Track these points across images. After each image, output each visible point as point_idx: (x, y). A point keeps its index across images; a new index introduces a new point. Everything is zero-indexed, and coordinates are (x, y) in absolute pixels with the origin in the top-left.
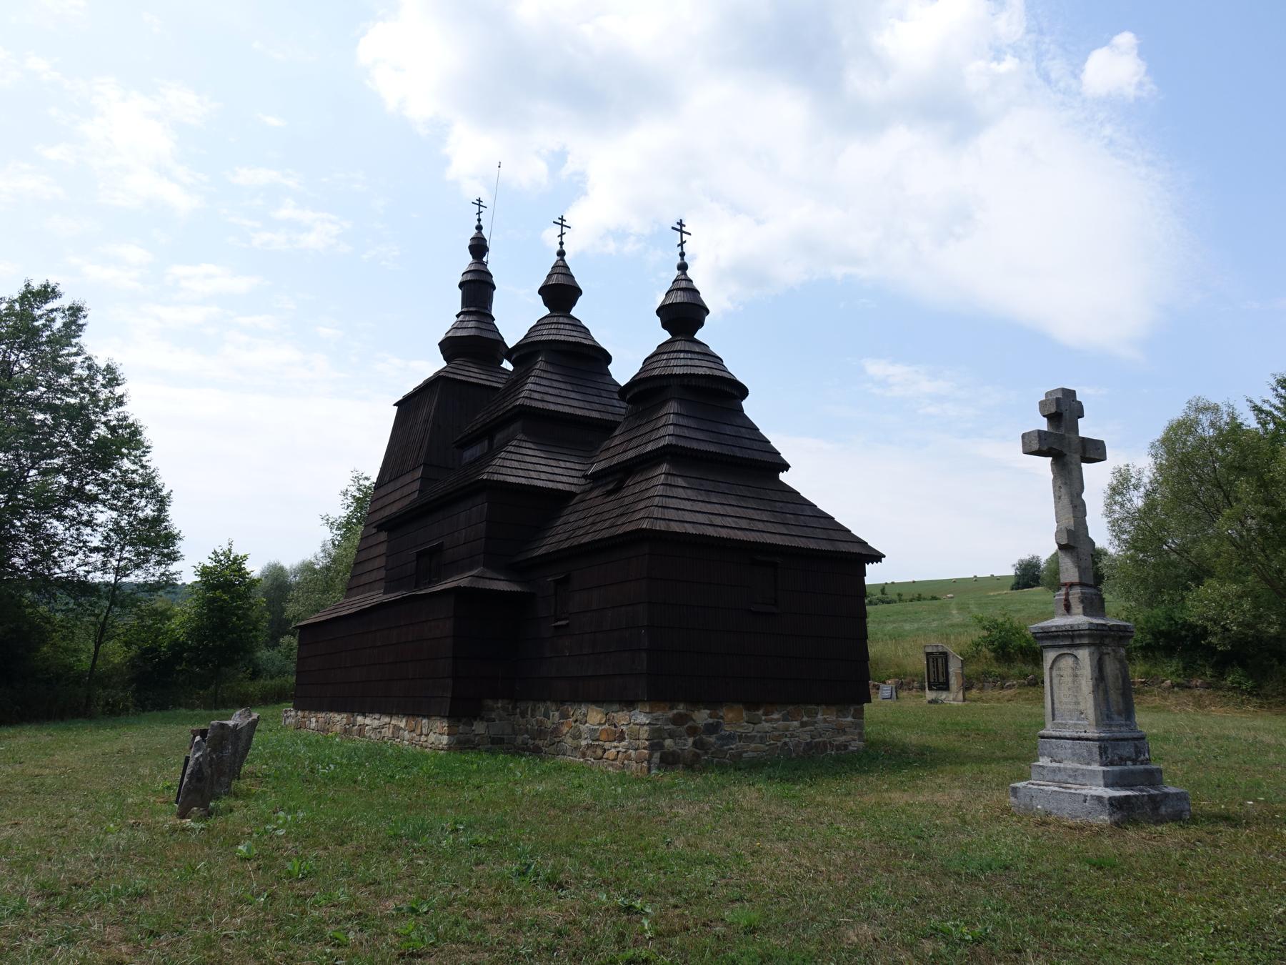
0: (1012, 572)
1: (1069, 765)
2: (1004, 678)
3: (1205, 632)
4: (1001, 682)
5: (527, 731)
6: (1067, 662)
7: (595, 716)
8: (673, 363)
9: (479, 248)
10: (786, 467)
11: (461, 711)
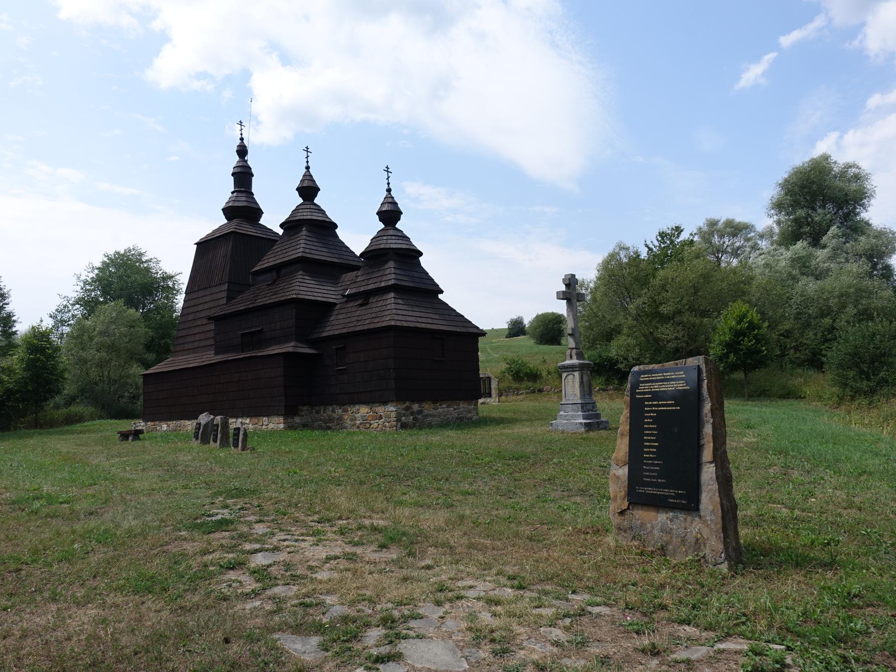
0: (506, 327)
1: (571, 413)
2: (518, 389)
3: (617, 362)
4: (517, 392)
5: (321, 420)
6: (571, 377)
7: (364, 410)
8: (390, 241)
9: (242, 151)
10: (442, 292)
11: (289, 412)
